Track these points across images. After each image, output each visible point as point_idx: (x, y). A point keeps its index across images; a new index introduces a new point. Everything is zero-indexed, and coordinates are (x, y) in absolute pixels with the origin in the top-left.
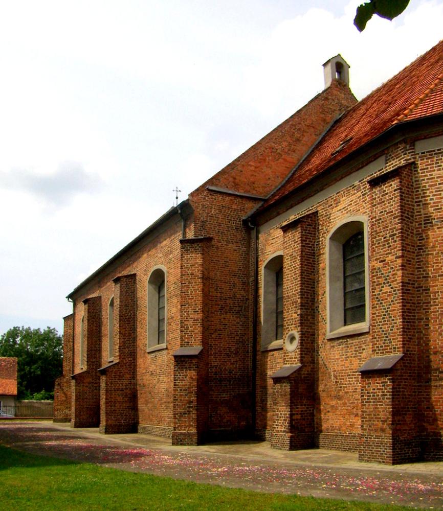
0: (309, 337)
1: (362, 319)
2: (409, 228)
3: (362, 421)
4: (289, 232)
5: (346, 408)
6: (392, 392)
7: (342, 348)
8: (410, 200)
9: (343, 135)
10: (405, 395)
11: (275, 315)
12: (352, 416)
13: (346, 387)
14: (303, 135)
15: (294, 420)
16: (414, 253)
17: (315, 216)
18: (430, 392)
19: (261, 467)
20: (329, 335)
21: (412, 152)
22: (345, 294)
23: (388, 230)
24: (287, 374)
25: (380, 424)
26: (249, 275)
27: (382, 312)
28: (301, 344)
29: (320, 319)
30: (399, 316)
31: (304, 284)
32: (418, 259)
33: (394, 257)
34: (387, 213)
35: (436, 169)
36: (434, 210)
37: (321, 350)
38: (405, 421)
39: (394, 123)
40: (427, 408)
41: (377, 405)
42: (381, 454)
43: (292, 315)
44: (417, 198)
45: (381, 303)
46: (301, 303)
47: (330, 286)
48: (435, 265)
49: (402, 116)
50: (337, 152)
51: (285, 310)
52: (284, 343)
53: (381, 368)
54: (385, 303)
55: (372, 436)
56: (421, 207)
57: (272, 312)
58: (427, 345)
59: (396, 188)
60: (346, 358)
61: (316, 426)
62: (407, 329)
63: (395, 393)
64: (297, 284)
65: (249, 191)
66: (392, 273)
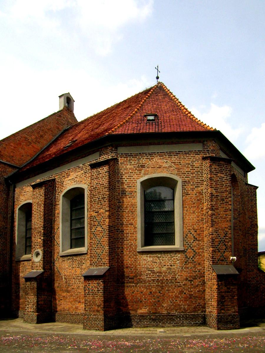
0: (48, 254)
1: (83, 245)
2: (113, 195)
3: (85, 306)
4: (37, 189)
5: (73, 297)
6: (104, 289)
7: (70, 262)
8: (114, 179)
9: (71, 138)
10: (110, 291)
11: (24, 239)
12: (76, 302)
13: (73, 285)
14: (45, 134)
15: (39, 304)
16: (115, 209)
17: (53, 181)
18: (124, 289)
19: (21, 336)
20: (61, 253)
21: (116, 152)
22: (71, 230)
23: (100, 195)
24: (35, 276)
25: (96, 308)
26: (8, 212)
27: (97, 242)
28: (44, 258)
29: (56, 243)
30: (107, 245)
31: (46, 221)
32: (117, 213)
33: (104, 210)
34: (100, 185)
35: (129, 164)
36: (127, 187)
37: (56, 262)
38: (111, 306)
39: (106, 134)
40: (122, 298)
41: (94, 296)
42: (97, 325)
43: (38, 239)
44: (117, 179)
45: (96, 237)
46: (44, 233)
47: (62, 225)
48: (127, 218)
49: (111, 131)
50: (67, 146)
51: (33, 236)
52: (32, 256)
53: (96, 274)
54: (98, 237)
55: (92, 314)
56: (120, 184)
57: (22, 237)
58: (122, 263)
59: (106, 171)
60: (72, 268)
61: (53, 308)
62: (111, 253)
63: (105, 290)
64: (41, 221)
65: (10, 161)
66: (103, 219)
